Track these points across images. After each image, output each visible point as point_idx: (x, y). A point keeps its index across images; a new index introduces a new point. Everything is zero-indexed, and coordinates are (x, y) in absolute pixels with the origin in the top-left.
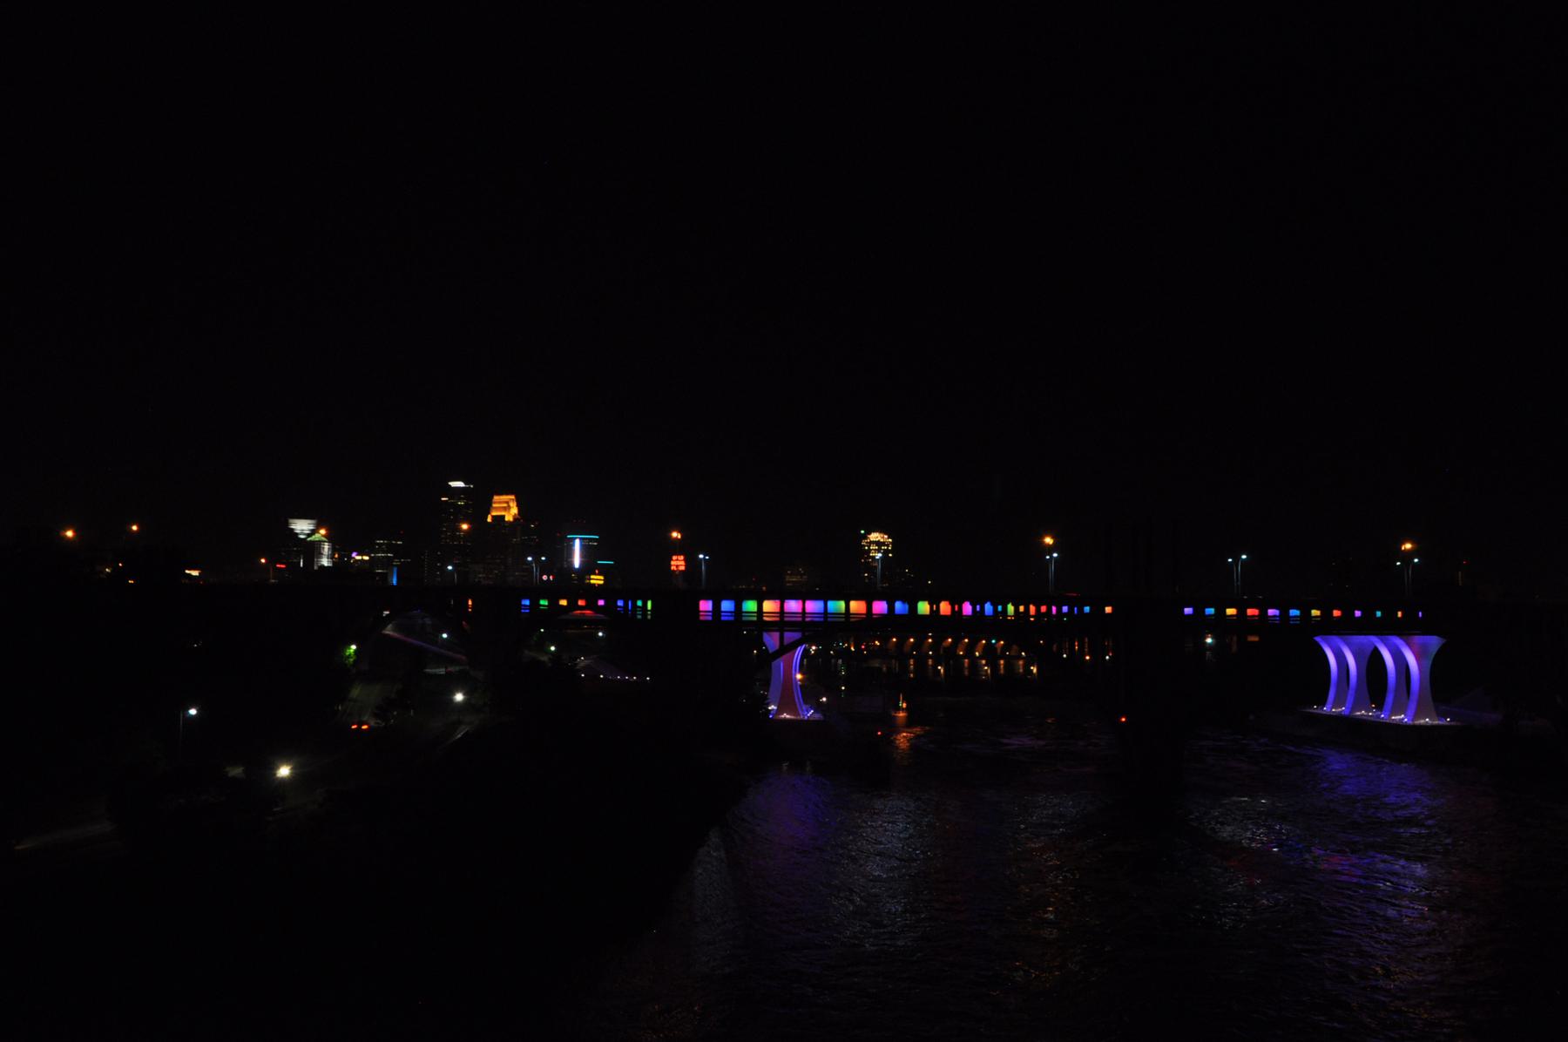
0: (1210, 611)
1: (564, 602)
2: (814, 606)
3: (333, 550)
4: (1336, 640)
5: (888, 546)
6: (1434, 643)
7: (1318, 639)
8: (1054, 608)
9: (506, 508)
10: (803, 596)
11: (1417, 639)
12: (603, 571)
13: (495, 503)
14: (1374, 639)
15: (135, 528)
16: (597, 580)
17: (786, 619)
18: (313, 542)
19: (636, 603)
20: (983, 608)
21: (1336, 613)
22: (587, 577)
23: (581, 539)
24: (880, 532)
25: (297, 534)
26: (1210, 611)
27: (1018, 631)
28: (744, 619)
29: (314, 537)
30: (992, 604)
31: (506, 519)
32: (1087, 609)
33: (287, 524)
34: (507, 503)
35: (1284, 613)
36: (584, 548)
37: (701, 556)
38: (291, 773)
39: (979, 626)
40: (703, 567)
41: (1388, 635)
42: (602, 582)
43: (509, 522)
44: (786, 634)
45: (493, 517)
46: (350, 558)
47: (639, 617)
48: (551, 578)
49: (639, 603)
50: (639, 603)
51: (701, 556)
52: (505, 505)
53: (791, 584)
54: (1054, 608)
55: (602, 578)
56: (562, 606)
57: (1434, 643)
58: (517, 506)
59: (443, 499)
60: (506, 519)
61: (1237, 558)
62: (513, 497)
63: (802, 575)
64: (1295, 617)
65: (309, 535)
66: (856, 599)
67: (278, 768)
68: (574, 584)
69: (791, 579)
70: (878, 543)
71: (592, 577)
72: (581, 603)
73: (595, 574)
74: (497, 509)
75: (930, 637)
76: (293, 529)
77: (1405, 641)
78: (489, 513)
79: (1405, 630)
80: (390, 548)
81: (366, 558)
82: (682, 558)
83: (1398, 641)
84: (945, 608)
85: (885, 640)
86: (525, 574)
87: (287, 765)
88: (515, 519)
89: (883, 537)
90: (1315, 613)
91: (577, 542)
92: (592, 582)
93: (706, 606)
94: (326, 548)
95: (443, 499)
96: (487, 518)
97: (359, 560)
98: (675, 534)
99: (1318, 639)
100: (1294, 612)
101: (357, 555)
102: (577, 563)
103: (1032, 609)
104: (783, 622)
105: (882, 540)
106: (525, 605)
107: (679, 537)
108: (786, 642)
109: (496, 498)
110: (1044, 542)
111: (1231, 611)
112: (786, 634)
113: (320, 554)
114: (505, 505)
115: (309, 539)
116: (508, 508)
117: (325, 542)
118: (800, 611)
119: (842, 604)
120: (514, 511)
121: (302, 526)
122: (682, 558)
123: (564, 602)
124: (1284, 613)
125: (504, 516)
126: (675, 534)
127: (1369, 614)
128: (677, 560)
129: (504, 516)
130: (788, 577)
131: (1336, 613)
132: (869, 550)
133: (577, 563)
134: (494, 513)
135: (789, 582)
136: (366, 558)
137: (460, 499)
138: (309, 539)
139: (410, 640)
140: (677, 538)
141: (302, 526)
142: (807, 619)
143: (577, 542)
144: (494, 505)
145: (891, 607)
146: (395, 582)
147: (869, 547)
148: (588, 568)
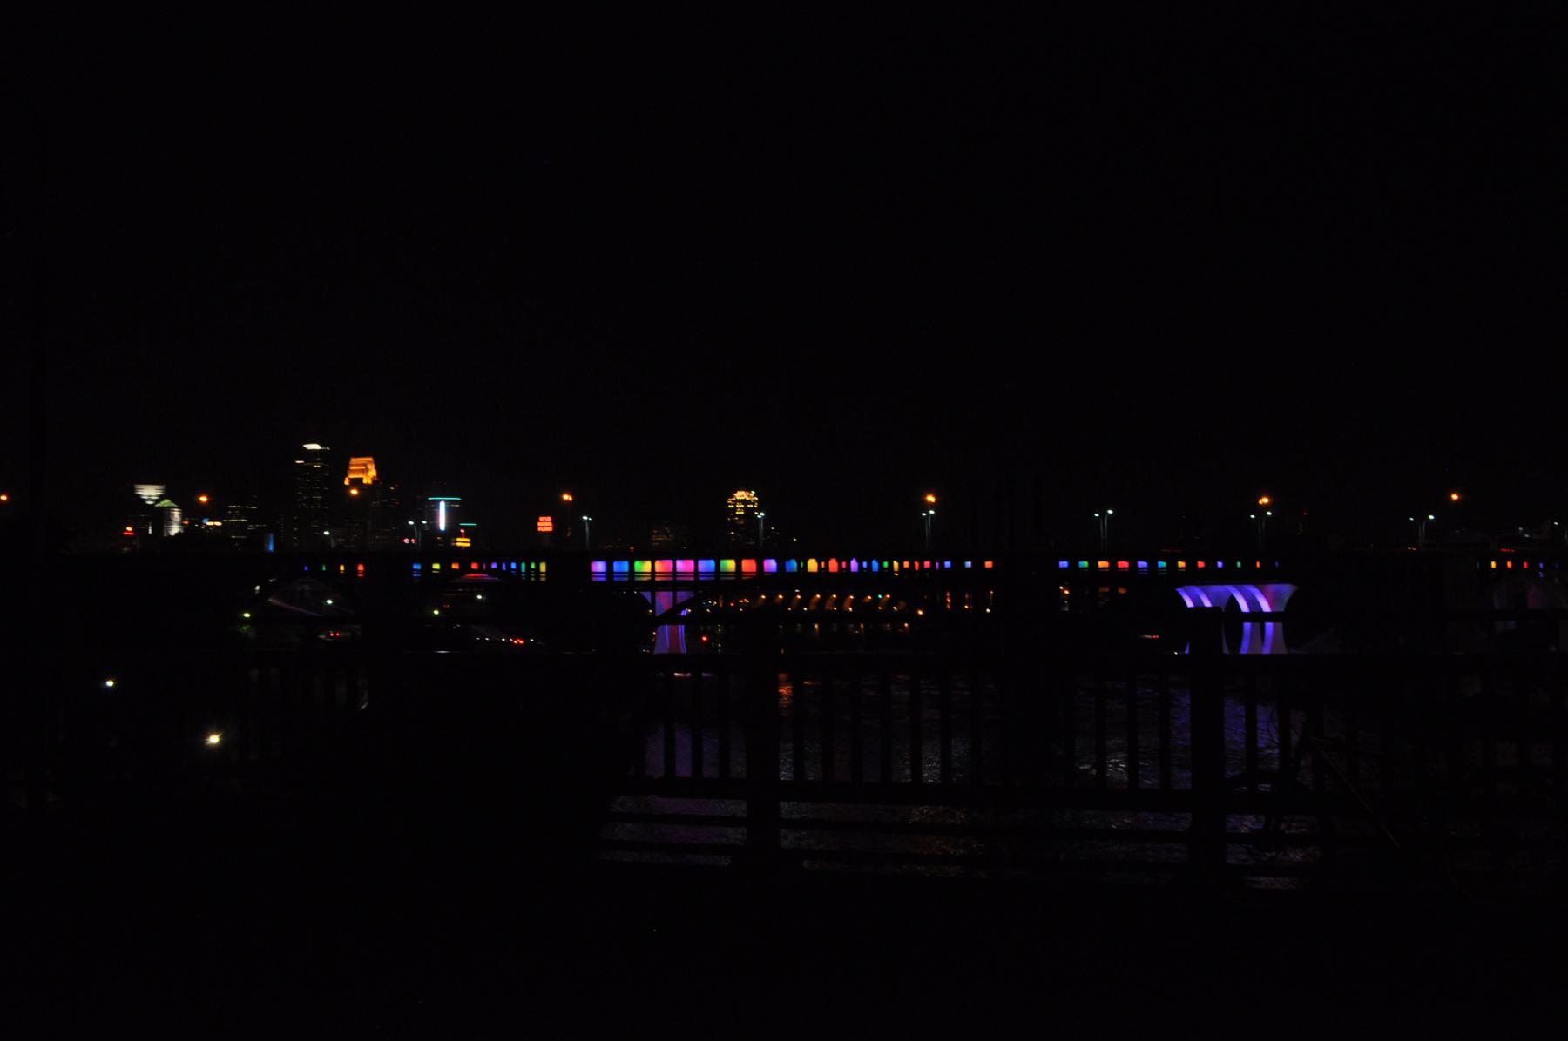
0: (1085, 564)
1: (455, 566)
2: (707, 565)
3: (183, 516)
4: (1196, 590)
5: (753, 504)
6: (1287, 590)
7: (1179, 590)
8: (916, 564)
9: (365, 471)
10: (674, 555)
11: (1271, 588)
12: (469, 533)
13: (353, 465)
14: (1231, 589)
15: (204, 499)
16: (463, 542)
17: (678, 579)
18: (162, 509)
19: (510, 565)
20: (849, 565)
21: (1201, 564)
22: (453, 539)
23: (445, 501)
24: (746, 491)
25: (144, 500)
26: (1085, 564)
27: (903, 586)
28: (637, 579)
29: (162, 503)
30: (857, 561)
31: (365, 482)
32: (947, 564)
33: (133, 490)
34: (365, 465)
35: (1153, 565)
36: (449, 511)
37: (585, 518)
38: (220, 741)
39: (866, 581)
40: (587, 529)
41: (1247, 583)
42: (468, 545)
43: (367, 485)
44: (678, 593)
45: (351, 479)
46: (201, 524)
47: (533, 579)
48: (413, 540)
49: (514, 566)
50: (514, 566)
51: (585, 518)
52: (363, 467)
53: (657, 544)
54: (916, 564)
55: (468, 540)
56: (1182, 561)
57: (1287, 590)
58: (376, 468)
59: (298, 462)
60: (365, 482)
61: (1103, 513)
62: (371, 459)
63: (667, 534)
64: (1163, 568)
65: (157, 501)
66: (661, 558)
67: (208, 736)
68: (438, 545)
69: (658, 539)
70: (744, 502)
71: (458, 539)
72: (474, 566)
73: (461, 537)
74: (354, 471)
75: (798, 594)
76: (139, 495)
77: (1259, 589)
78: (346, 476)
79: (1260, 579)
80: (244, 513)
81: (219, 524)
82: (549, 519)
83: (1253, 590)
84: (833, 565)
85: (754, 597)
86: (386, 537)
87: (217, 734)
88: (374, 482)
89: (749, 496)
90: (1181, 564)
91: (442, 506)
92: (458, 544)
93: (600, 567)
94: (176, 514)
95: (298, 462)
96: (344, 480)
97: (210, 526)
98: (566, 497)
99: (1179, 590)
100: (1142, 564)
101: (209, 521)
102: (442, 526)
103: (896, 564)
104: (674, 582)
105: (748, 499)
106: (416, 570)
107: (571, 499)
108: (679, 601)
109: (353, 460)
110: (926, 500)
111: (1103, 564)
112: (678, 593)
113: (170, 521)
114: (363, 467)
115: (157, 505)
116: (366, 471)
117: (175, 508)
118: (671, 570)
119: (712, 563)
120: (373, 473)
121: (149, 492)
122: (549, 519)
123: (455, 566)
124: (1153, 565)
125: (361, 479)
126: (566, 497)
127: (1249, 564)
128: (544, 521)
129: (361, 479)
130: (654, 536)
131: (1201, 564)
132: (735, 509)
133: (442, 526)
134: (351, 476)
135: (655, 541)
136: (219, 524)
137: (316, 463)
138: (157, 505)
139: (293, 608)
140: (568, 501)
141: (149, 492)
142: (657, 579)
143: (442, 506)
144: (352, 468)
145: (760, 566)
146: (271, 548)
147: (735, 505)
148: (453, 531)
